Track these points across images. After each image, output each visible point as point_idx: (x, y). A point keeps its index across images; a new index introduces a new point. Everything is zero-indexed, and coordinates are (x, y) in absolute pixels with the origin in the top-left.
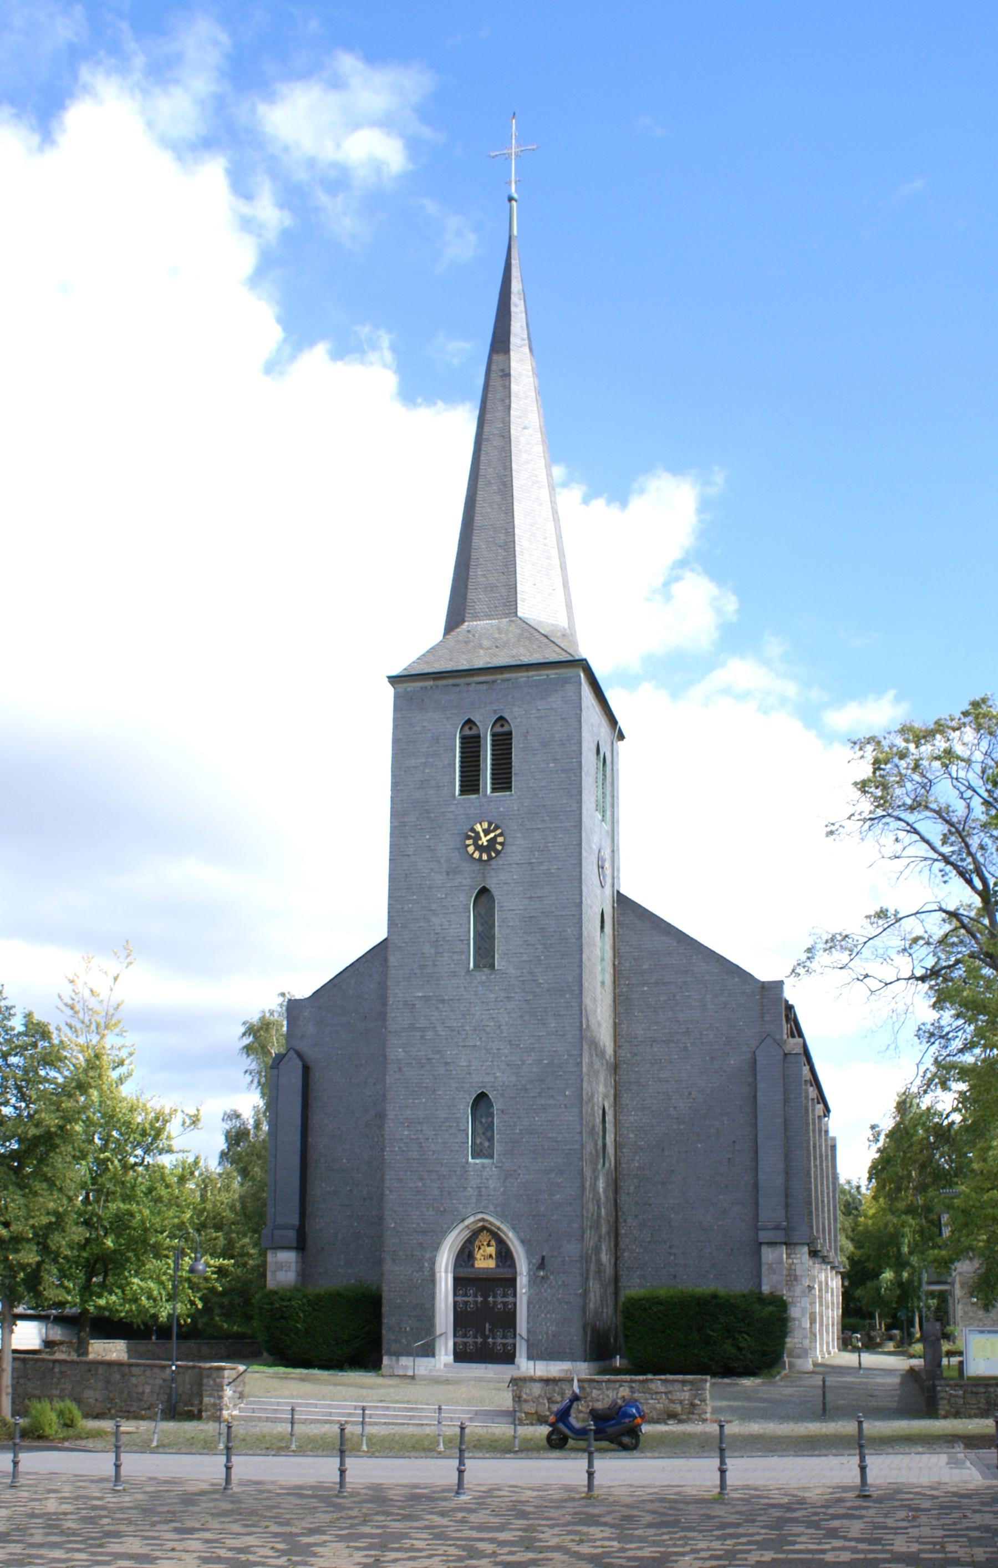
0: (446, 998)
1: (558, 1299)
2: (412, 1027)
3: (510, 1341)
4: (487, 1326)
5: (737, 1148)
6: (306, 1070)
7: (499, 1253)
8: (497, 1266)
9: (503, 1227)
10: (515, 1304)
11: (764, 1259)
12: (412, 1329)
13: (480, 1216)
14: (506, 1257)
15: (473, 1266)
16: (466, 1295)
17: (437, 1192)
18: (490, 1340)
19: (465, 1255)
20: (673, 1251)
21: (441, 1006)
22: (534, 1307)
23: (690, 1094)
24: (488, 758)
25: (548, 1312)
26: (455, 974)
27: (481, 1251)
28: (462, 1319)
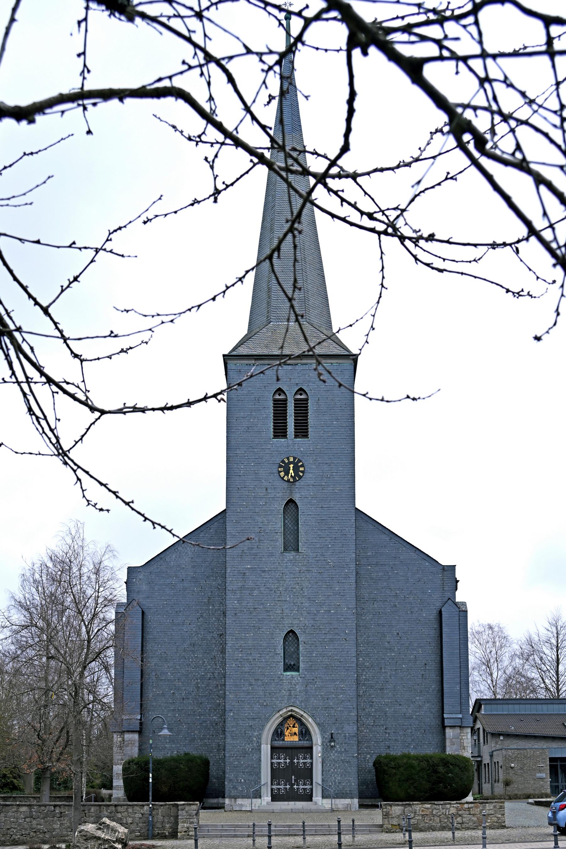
0: (267, 569)
1: (341, 760)
2: (242, 588)
3: (308, 787)
4: (293, 777)
5: (427, 668)
6: (143, 613)
8: (300, 740)
9: (305, 715)
11: (447, 736)
12: (245, 781)
13: (290, 708)
14: (306, 733)
15: (283, 740)
16: (279, 759)
17: (261, 693)
18: (295, 787)
19: (278, 733)
20: (388, 731)
21: (263, 574)
22: (326, 765)
23: (398, 634)
24: (291, 416)
25: (335, 768)
26: (271, 555)
27: (289, 730)
28: (276, 774)
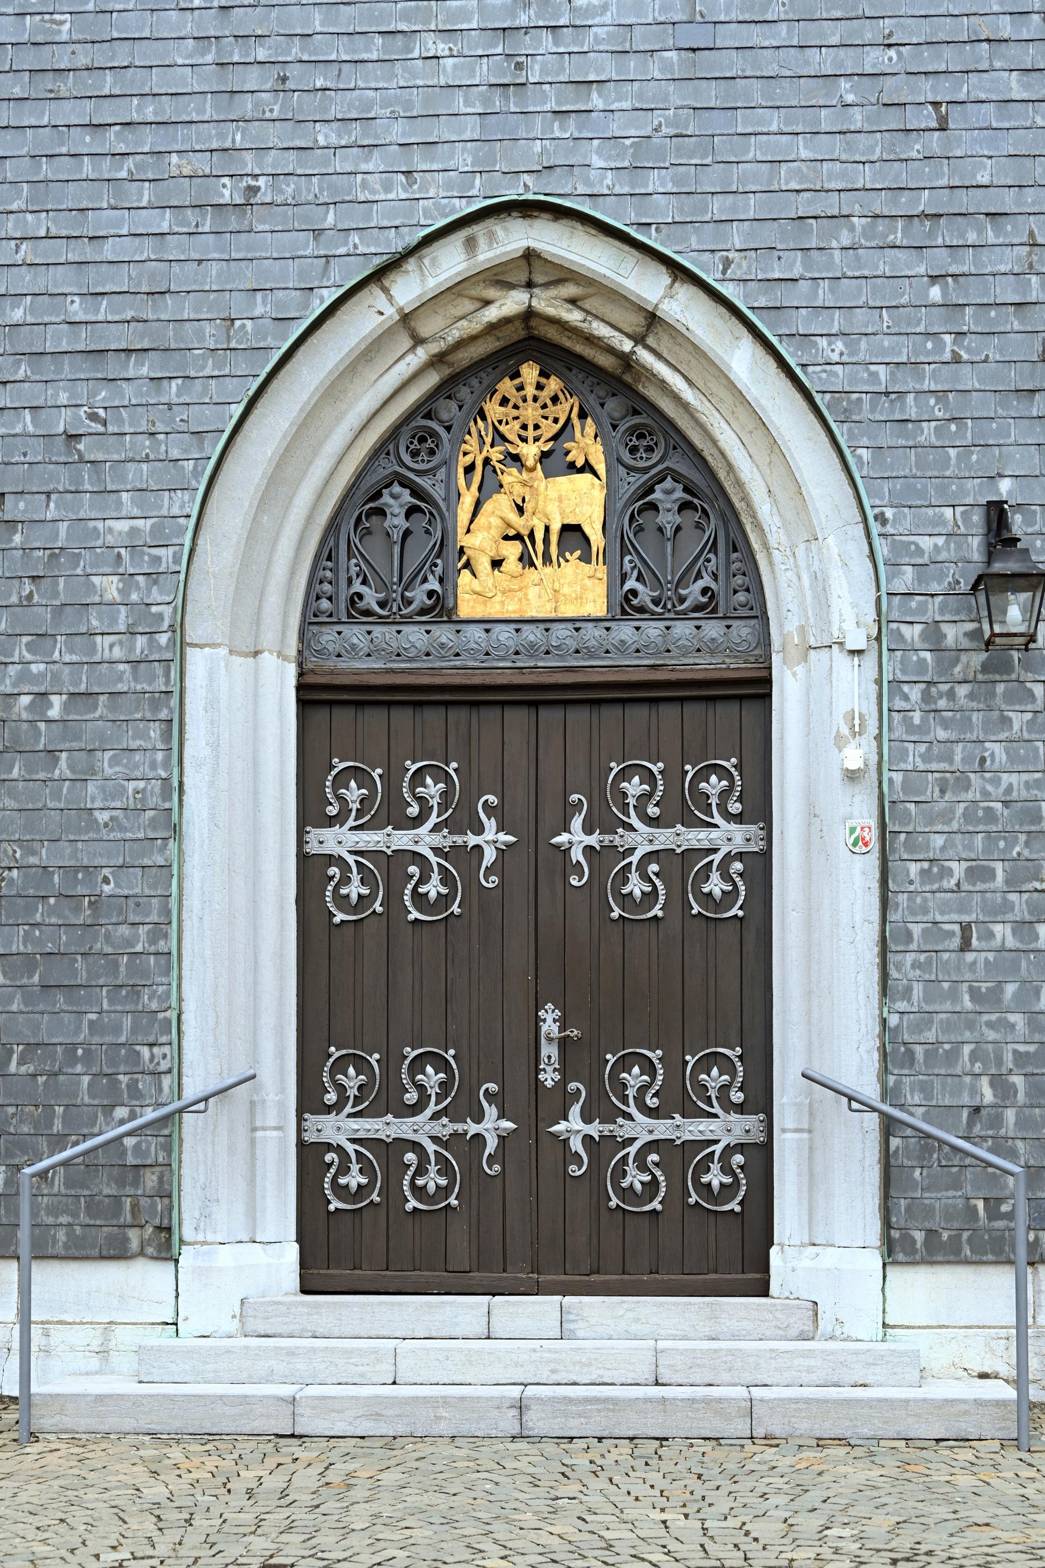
4: (550, 1022)
7: (632, 513)
8: (626, 607)
10: (759, 866)
15: (440, 609)
18: (573, 1126)
19: (388, 521)
27: (499, 506)
28: (356, 984)
